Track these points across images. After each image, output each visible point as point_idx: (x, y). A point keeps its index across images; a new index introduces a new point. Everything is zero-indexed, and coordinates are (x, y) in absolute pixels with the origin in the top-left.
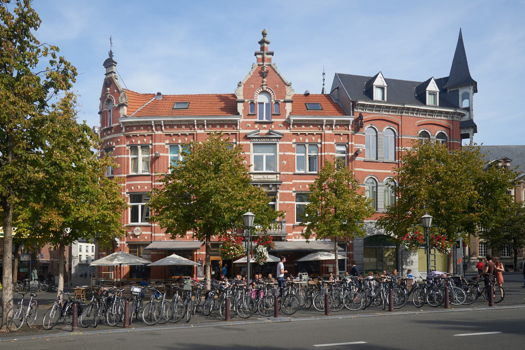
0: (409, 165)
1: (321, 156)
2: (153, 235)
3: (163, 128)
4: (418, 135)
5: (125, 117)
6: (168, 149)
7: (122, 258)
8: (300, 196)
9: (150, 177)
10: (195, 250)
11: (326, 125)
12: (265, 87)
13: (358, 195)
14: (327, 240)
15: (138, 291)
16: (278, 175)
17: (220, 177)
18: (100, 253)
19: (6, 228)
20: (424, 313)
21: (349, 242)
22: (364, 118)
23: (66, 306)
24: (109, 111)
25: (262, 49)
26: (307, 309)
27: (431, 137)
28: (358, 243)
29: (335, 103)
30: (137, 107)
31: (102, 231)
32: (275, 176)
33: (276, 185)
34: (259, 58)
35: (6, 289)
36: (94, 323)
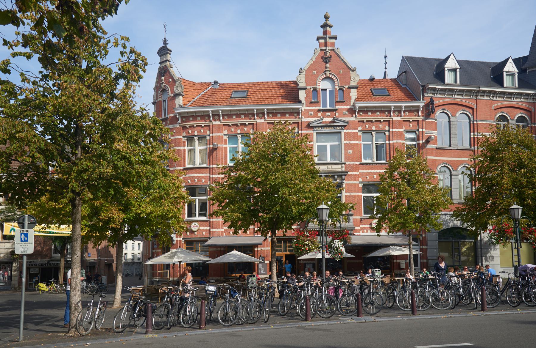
0: (487, 152)
1: (390, 144)
2: (211, 230)
3: (221, 118)
4: (495, 119)
5: (181, 107)
6: (226, 140)
7: (182, 255)
8: (367, 187)
9: (208, 169)
10: (256, 245)
11: (394, 112)
12: (328, 73)
13: (433, 185)
14: (398, 234)
15: (213, 290)
16: (343, 165)
17: (288, 169)
18: (154, 251)
19: (75, 226)
20: (520, 313)
21: (421, 235)
22: (435, 102)
23: (136, 306)
24: (164, 101)
25: (325, 33)
26: (389, 308)
27: (510, 121)
28: (433, 236)
29: (403, 88)
30: (193, 97)
31: (162, 227)
32: (340, 166)
33: (341, 175)
34: (321, 43)
35: (74, 289)
36: (167, 325)
